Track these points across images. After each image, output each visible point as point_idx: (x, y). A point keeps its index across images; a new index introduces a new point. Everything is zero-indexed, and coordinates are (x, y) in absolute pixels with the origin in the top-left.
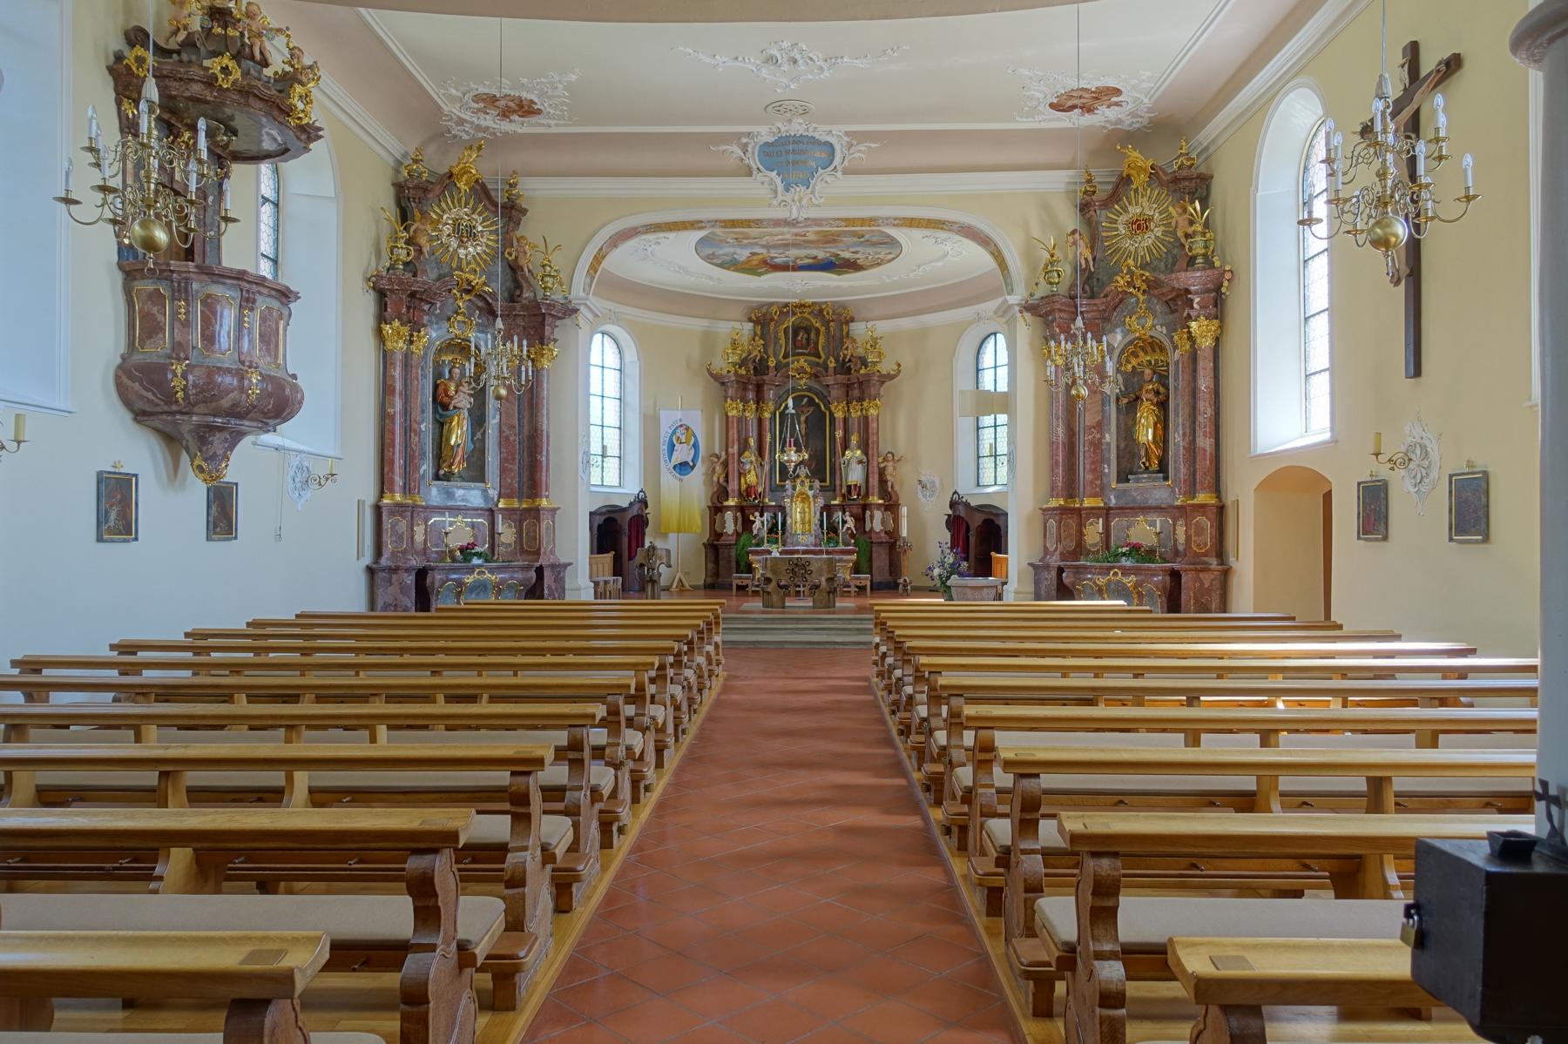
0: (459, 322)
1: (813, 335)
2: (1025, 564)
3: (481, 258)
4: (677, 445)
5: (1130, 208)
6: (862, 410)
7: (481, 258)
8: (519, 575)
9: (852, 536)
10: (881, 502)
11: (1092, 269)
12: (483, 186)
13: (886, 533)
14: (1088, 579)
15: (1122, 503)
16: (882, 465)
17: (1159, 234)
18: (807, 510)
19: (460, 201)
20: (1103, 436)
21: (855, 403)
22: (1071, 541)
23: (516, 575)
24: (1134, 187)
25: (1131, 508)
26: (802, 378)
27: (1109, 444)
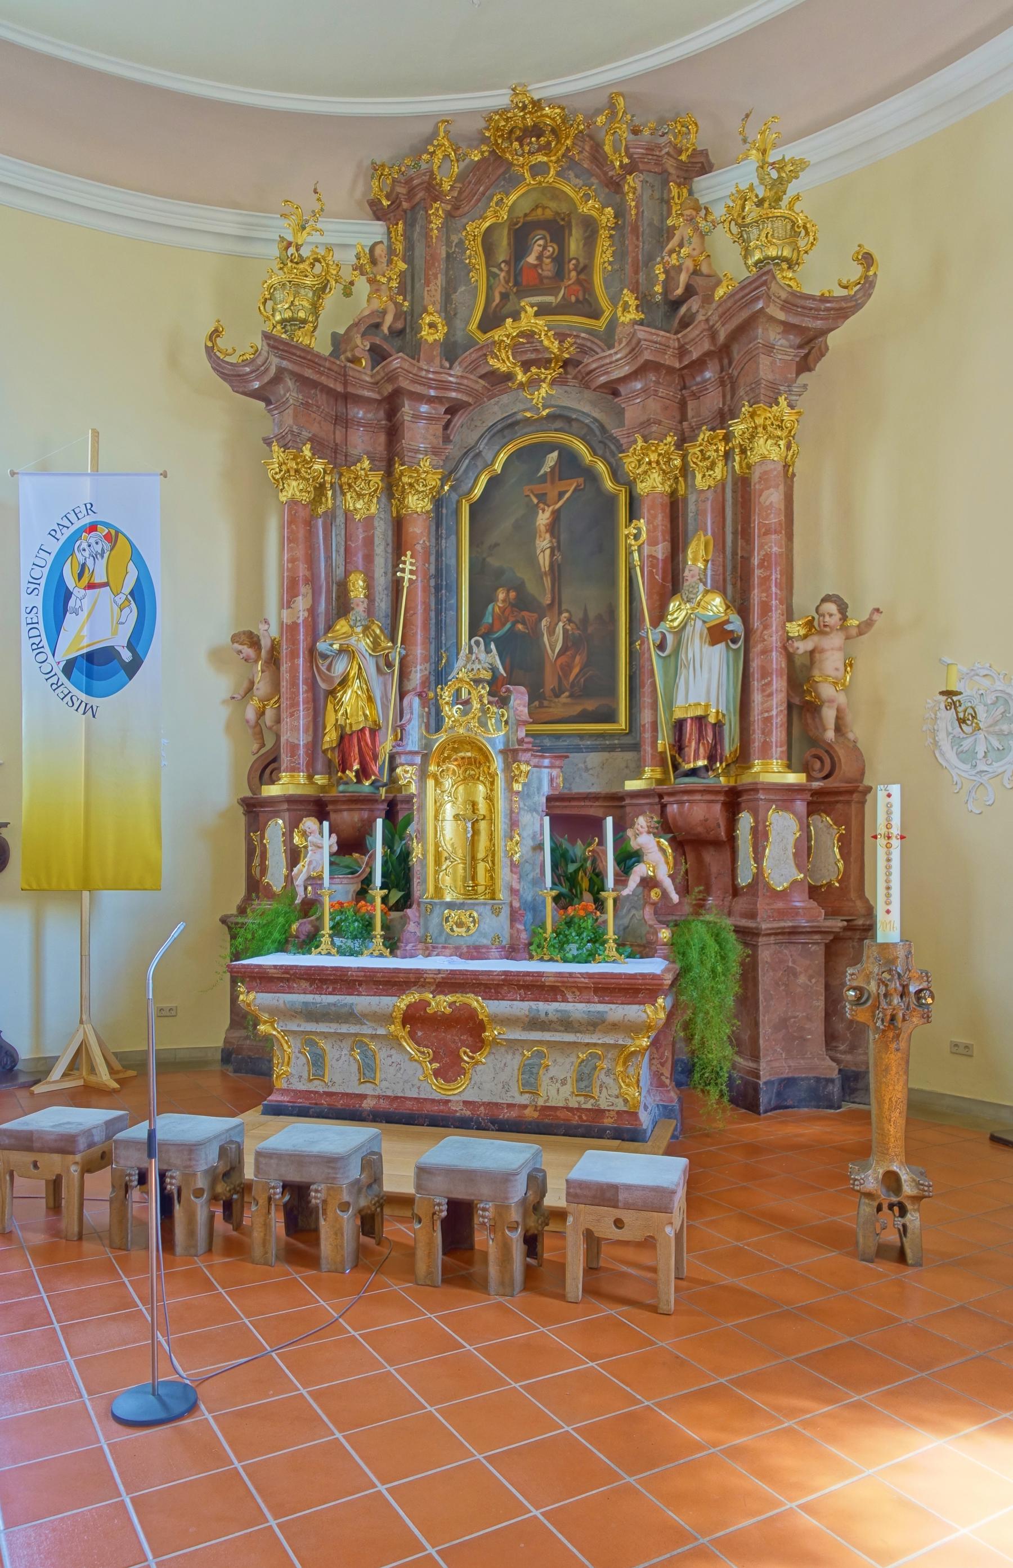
1: (574, 246)
4: (78, 592)
6: (728, 455)
9: (664, 911)
10: (793, 778)
13: (813, 892)
16: (803, 647)
18: (482, 808)
21: (704, 435)
26: (534, 383)
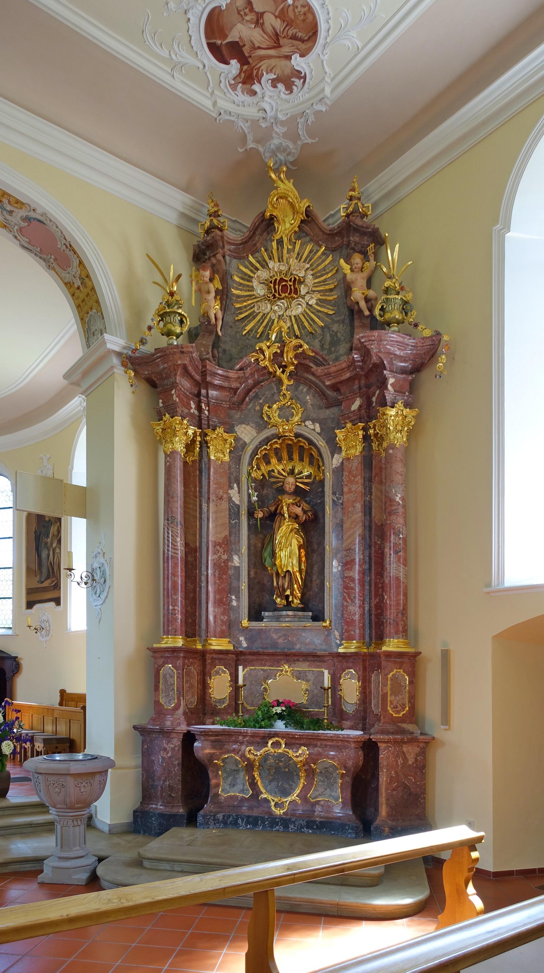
2: (126, 726)
5: (271, 264)
11: (220, 333)
14: (234, 751)
15: (256, 647)
17: (313, 302)
20: (230, 559)
22: (193, 696)
24: (277, 237)
25: (269, 654)
27: (237, 569)
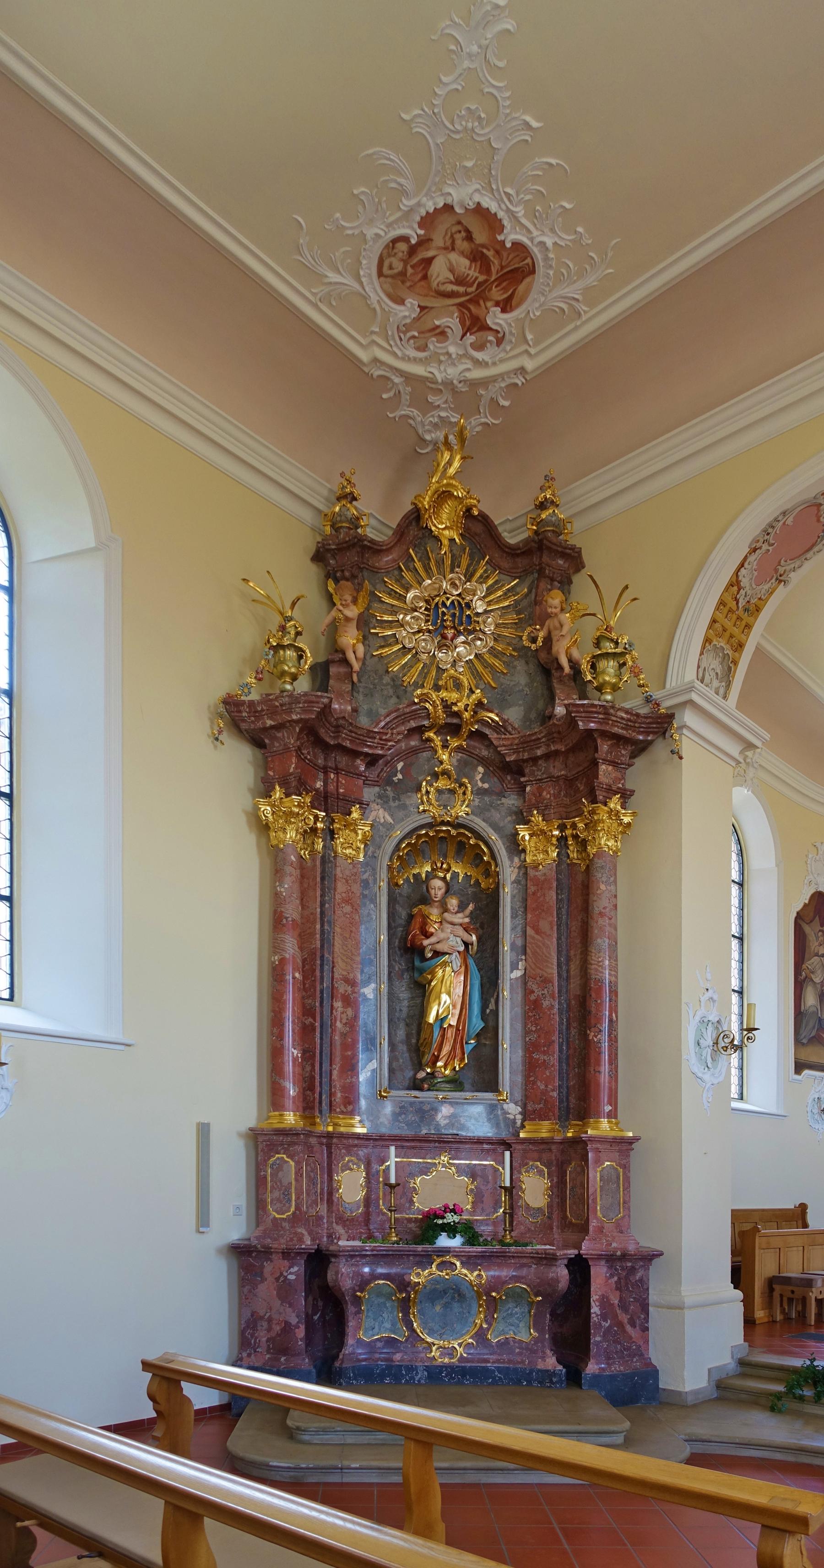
0: (439, 791)
3: (486, 665)
7: (486, 665)
8: (532, 1272)
12: (484, 520)
19: (440, 563)
23: (524, 1272)
